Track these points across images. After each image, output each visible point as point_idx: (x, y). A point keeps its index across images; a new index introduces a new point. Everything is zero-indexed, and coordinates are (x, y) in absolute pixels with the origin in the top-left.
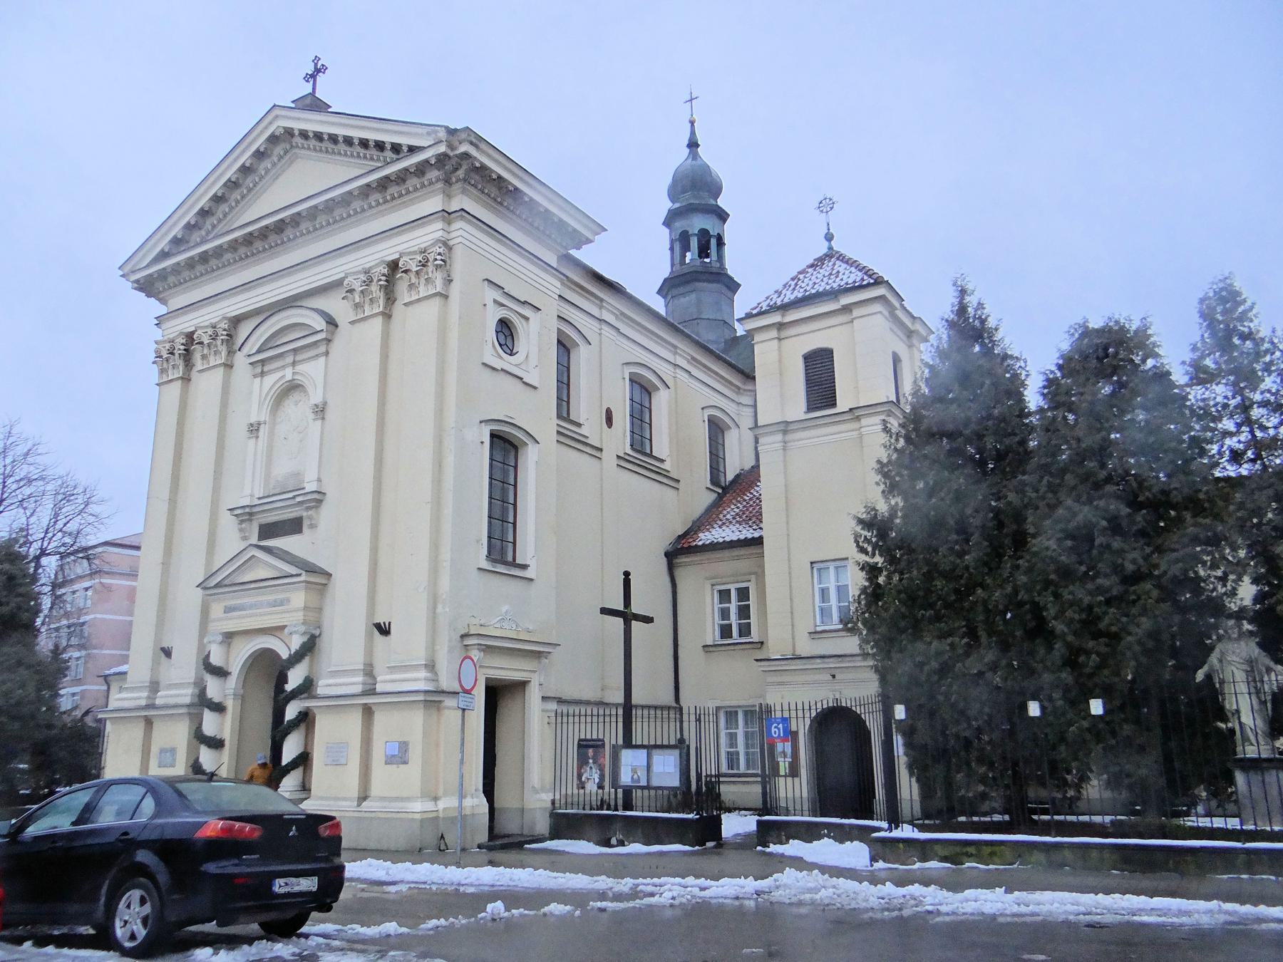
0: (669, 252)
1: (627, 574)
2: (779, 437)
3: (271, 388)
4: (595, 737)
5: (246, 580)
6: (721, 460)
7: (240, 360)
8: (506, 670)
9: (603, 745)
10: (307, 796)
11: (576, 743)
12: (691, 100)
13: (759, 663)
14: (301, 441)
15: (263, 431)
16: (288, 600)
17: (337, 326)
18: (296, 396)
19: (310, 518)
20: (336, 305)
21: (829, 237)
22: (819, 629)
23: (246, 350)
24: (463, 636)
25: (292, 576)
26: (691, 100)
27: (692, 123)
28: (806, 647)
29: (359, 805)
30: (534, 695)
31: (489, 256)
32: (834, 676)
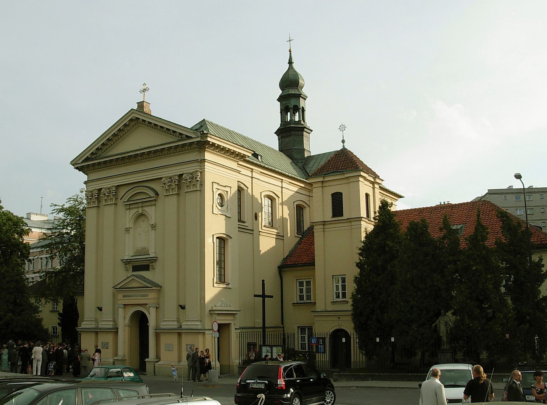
0: (280, 113)
1: (263, 281)
2: (322, 227)
3: (133, 216)
4: (253, 342)
5: (130, 286)
6: (302, 216)
7: (120, 202)
8: (223, 320)
9: (256, 345)
10: (159, 360)
11: (247, 343)
12: (290, 41)
13: (313, 313)
14: (146, 236)
15: (131, 231)
16: (147, 295)
17: (158, 195)
18: (142, 218)
19: (153, 266)
20: (156, 186)
21: (343, 141)
22: (335, 300)
23: (123, 200)
24: (210, 311)
25: (148, 287)
26: (290, 41)
27: (290, 51)
28: (330, 308)
29: (178, 364)
30: (233, 328)
31: (214, 172)
32: (339, 318)
